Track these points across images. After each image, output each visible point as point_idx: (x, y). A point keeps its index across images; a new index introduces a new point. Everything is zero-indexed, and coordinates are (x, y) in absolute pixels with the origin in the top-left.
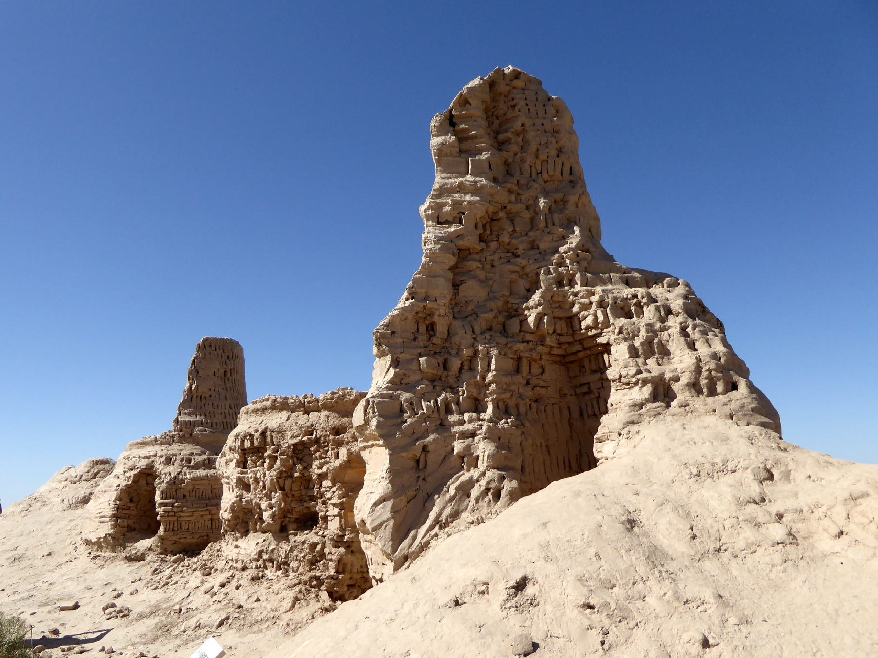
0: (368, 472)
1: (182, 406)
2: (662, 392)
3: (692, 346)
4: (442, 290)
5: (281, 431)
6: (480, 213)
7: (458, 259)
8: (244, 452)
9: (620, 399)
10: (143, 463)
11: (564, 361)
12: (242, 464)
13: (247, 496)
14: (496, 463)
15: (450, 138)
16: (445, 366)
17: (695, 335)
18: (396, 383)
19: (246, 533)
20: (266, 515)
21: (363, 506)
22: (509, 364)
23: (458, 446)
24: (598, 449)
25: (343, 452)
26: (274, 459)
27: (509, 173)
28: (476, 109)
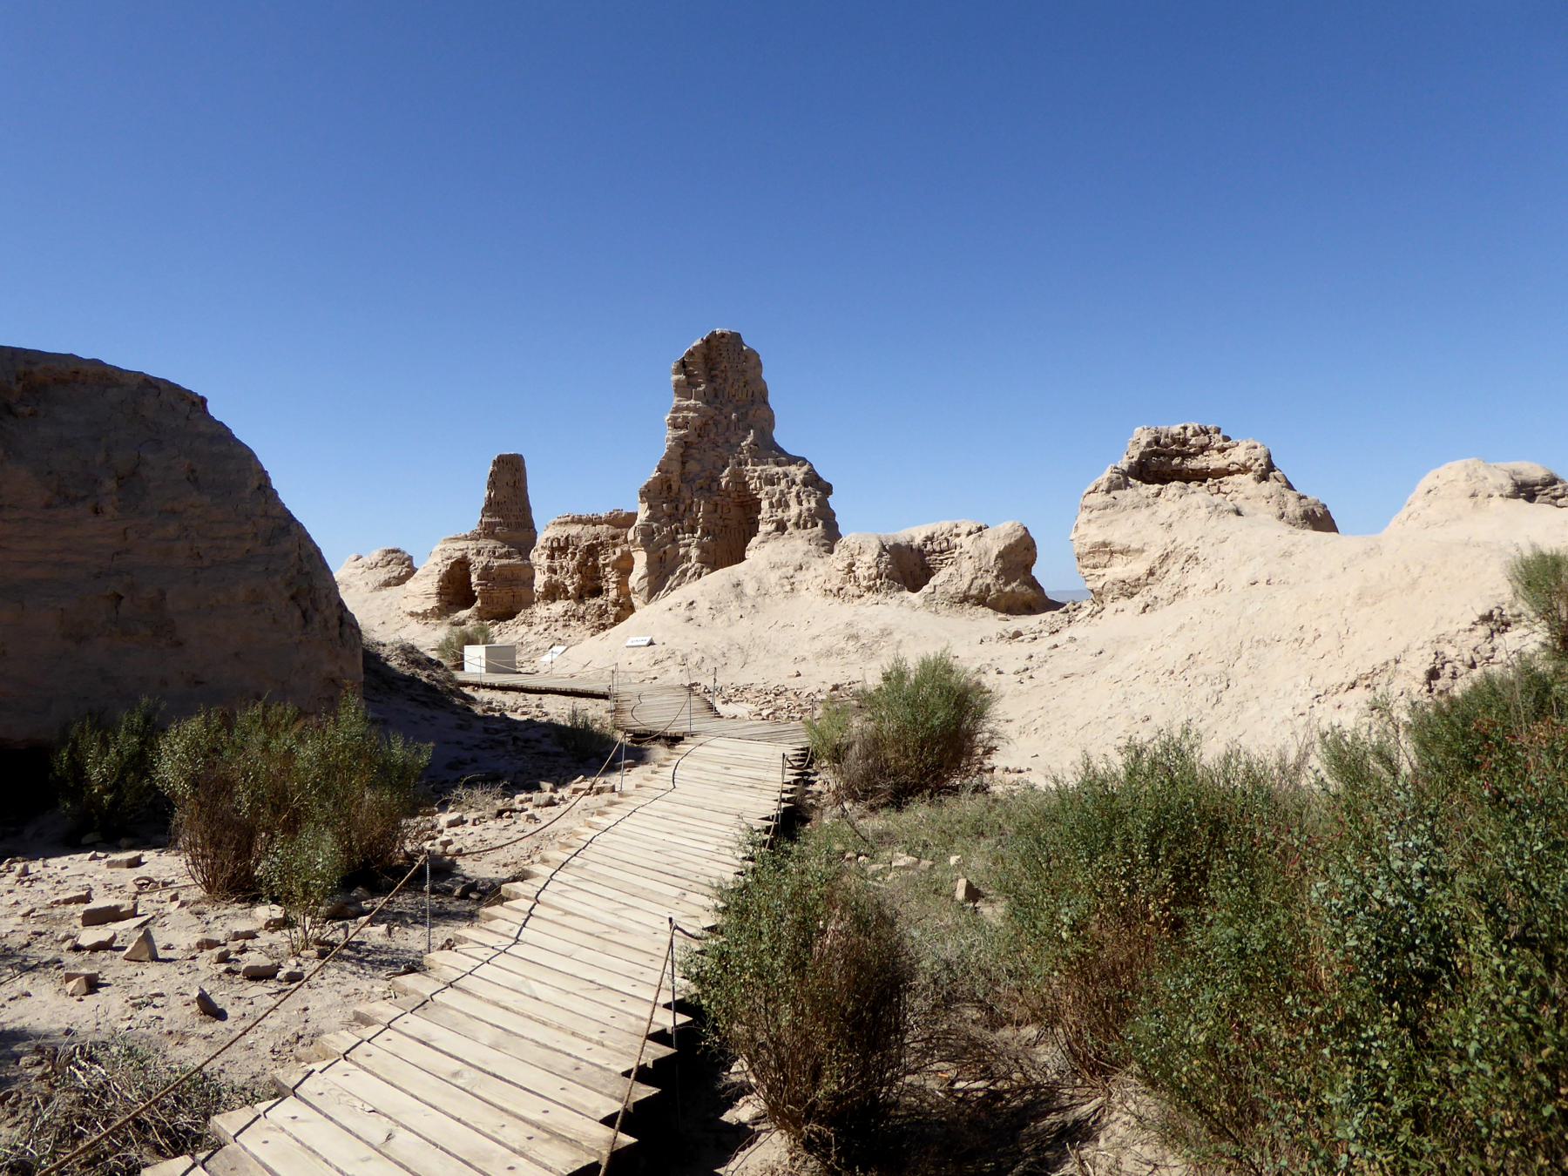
0: (437, 578)
1: (485, 510)
2: (781, 527)
3: (800, 503)
4: (676, 467)
5: (578, 537)
6: (698, 423)
7: (684, 450)
8: (553, 550)
9: (764, 528)
10: (458, 554)
11: (742, 505)
12: (551, 557)
13: (555, 577)
14: (700, 560)
15: (682, 377)
16: (677, 508)
17: (803, 497)
18: (650, 518)
19: (554, 601)
20: (570, 589)
21: (633, 580)
22: (711, 507)
23: (682, 551)
24: (748, 554)
25: (618, 551)
26: (574, 554)
27: (716, 396)
28: (698, 358)
